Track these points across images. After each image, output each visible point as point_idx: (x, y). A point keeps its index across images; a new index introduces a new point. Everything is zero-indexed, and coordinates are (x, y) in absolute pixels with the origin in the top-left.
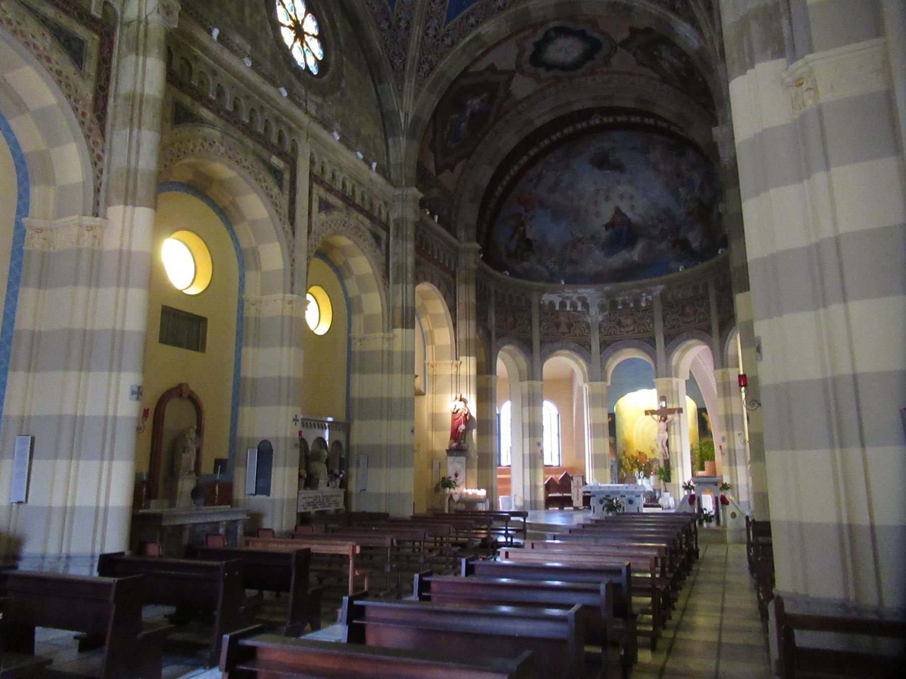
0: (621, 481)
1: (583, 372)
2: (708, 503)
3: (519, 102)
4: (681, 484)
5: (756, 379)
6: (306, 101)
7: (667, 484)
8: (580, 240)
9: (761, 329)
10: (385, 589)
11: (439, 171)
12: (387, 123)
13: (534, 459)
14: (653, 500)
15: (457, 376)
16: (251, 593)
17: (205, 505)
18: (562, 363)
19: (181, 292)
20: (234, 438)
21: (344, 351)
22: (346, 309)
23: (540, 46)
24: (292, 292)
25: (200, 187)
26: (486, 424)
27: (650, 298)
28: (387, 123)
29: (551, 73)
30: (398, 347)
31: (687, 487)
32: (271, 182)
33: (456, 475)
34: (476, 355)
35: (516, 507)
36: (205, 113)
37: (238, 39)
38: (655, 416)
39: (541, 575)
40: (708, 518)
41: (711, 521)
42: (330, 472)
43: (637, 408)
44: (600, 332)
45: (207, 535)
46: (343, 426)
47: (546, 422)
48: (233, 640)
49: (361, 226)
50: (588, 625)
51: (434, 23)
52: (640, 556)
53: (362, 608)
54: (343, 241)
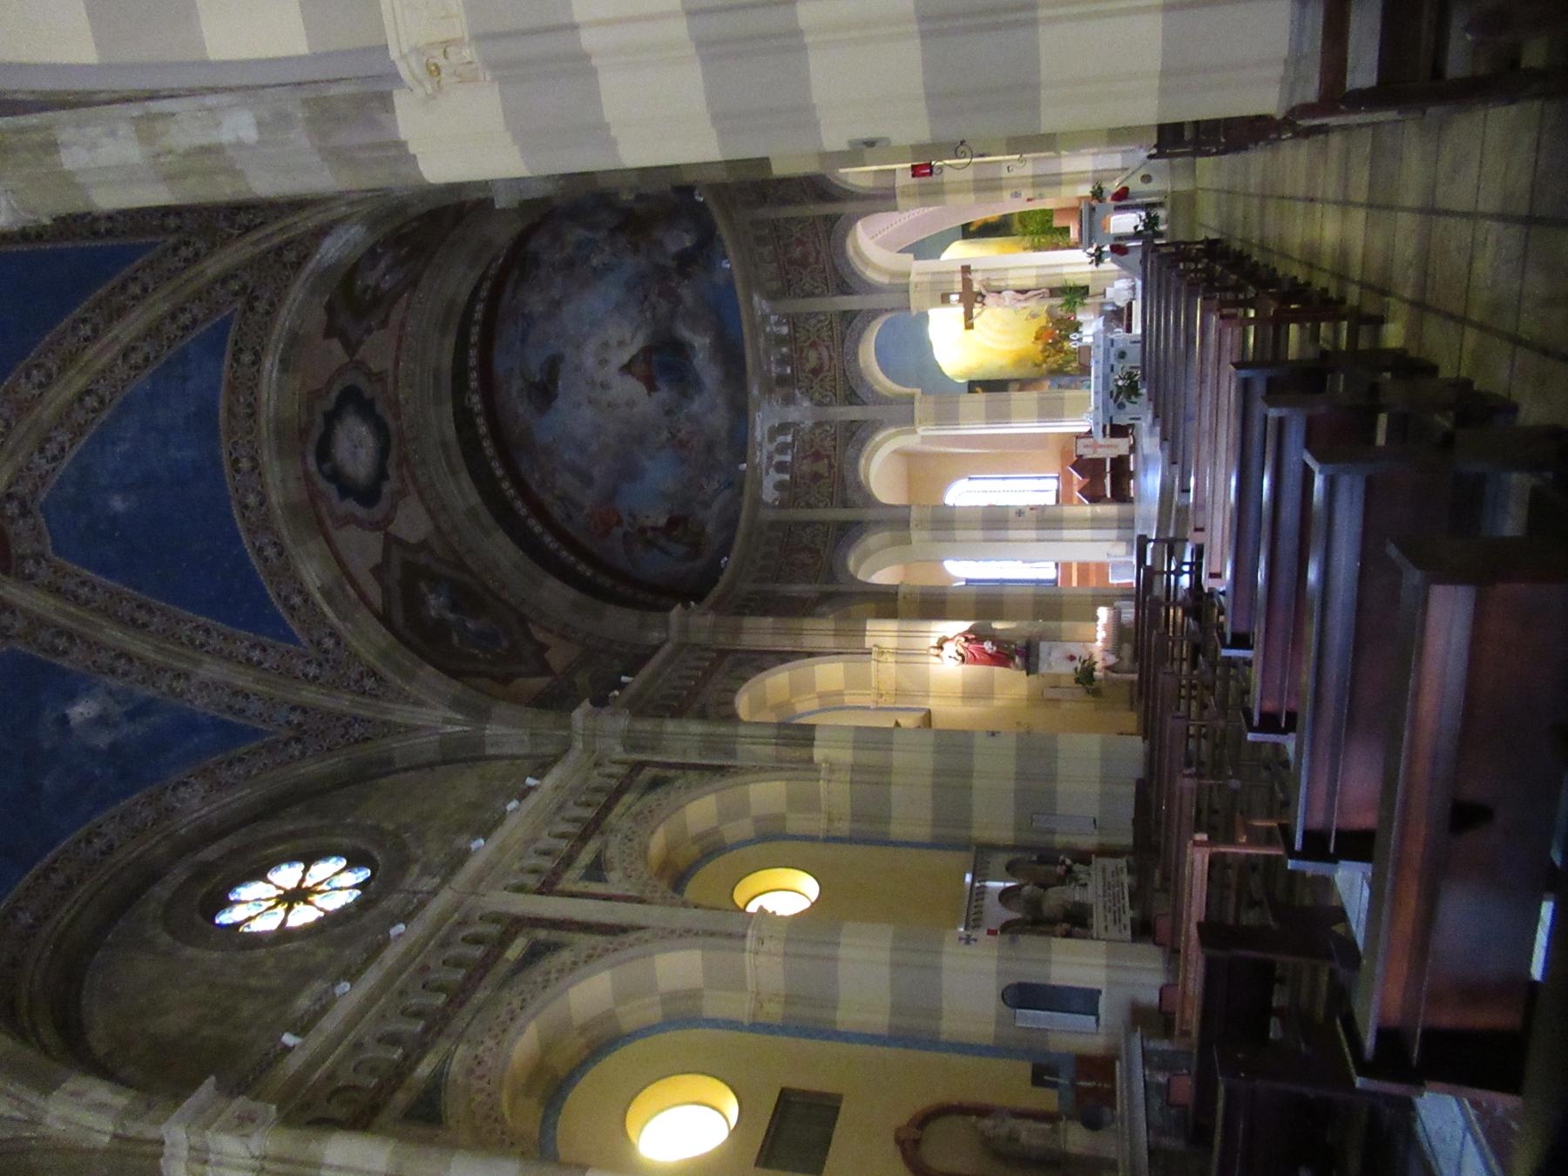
0: (1085, 370)
1: (899, 434)
2: (1125, 222)
3: (438, 528)
4: (1093, 267)
5: (918, 149)
6: (415, 893)
7: (1091, 292)
8: (674, 436)
9: (835, 139)
10: (1272, 788)
11: (545, 669)
12: (461, 755)
13: (1045, 521)
14: (1119, 316)
15: (898, 652)
16: (1275, 1030)
17: (1113, 1107)
18: (880, 472)
19: (733, 1133)
20: (996, 1050)
21: (849, 850)
22: (776, 843)
23: (346, 488)
24: (744, 936)
25: (553, 1085)
26: (984, 603)
27: (773, 318)
28: (461, 755)
29: (392, 471)
30: (846, 756)
31: (1098, 258)
32: (552, 962)
33: (1072, 658)
34: (863, 619)
35: (1129, 554)
36: (424, 1069)
37: (303, 1002)
38: (975, 311)
39: (1252, 513)
40: (1151, 222)
41: (1156, 217)
42: (1061, 881)
43: (962, 344)
44: (830, 404)
45: (1170, 1105)
46: (982, 855)
47: (983, 500)
48: (1365, 1069)
49: (634, 809)
50: (1338, 439)
51: (298, 665)
52: (1217, 343)
53: (1307, 834)
54: (657, 842)
